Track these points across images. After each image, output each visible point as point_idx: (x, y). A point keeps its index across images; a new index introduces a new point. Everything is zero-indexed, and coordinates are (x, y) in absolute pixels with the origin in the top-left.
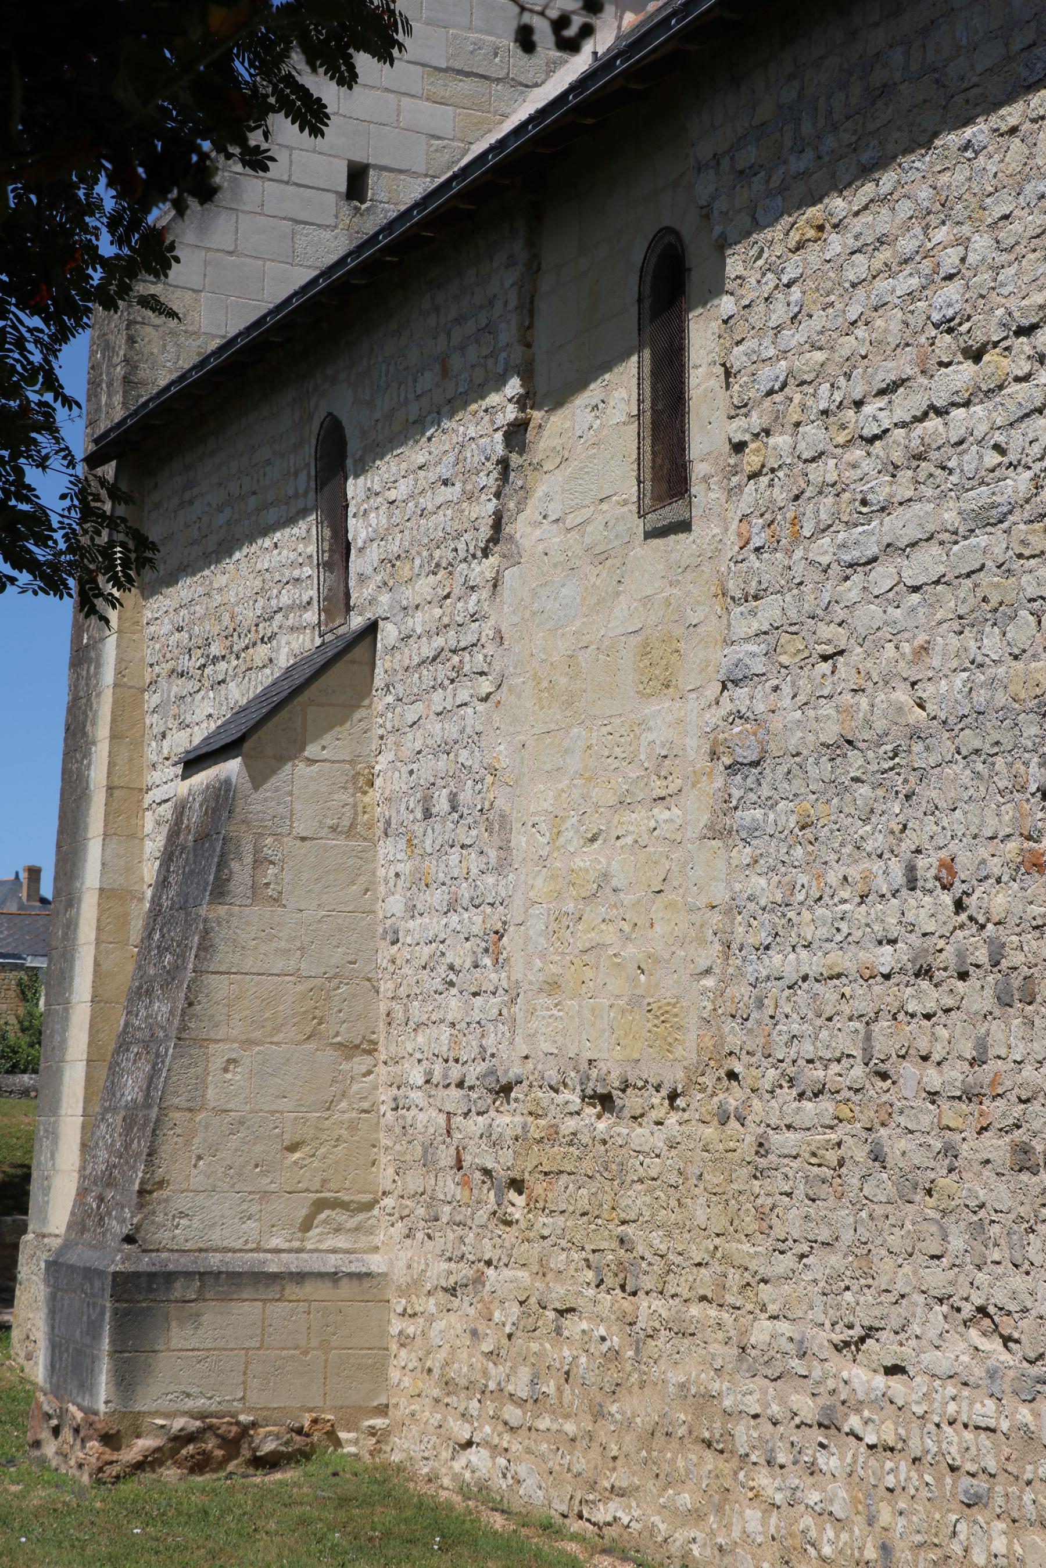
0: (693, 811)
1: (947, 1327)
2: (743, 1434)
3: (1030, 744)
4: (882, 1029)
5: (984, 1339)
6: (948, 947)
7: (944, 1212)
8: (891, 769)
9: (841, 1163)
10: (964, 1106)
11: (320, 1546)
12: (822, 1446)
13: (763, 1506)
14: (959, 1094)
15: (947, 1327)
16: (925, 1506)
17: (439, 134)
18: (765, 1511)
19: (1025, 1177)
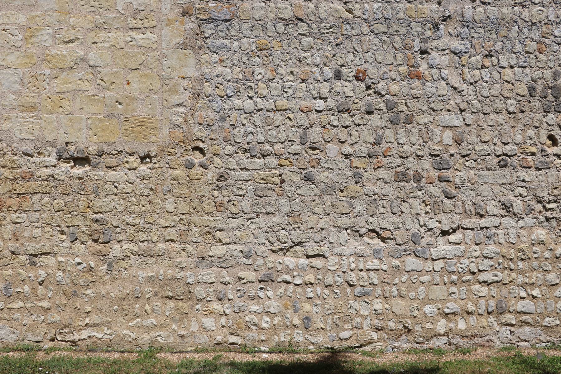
0: (171, 36)
1: (349, 238)
2: (200, 291)
3: (416, 34)
4: (315, 132)
5: (370, 240)
6: (360, 102)
7: (351, 198)
8: (327, 33)
9: (282, 181)
10: (367, 160)
11: (493, 208)
12: (262, 288)
13: (215, 316)
14: (365, 155)
15: (349, 238)
16: (333, 301)
17: (530, 312)
18: (215, 318)
19: (402, 183)
